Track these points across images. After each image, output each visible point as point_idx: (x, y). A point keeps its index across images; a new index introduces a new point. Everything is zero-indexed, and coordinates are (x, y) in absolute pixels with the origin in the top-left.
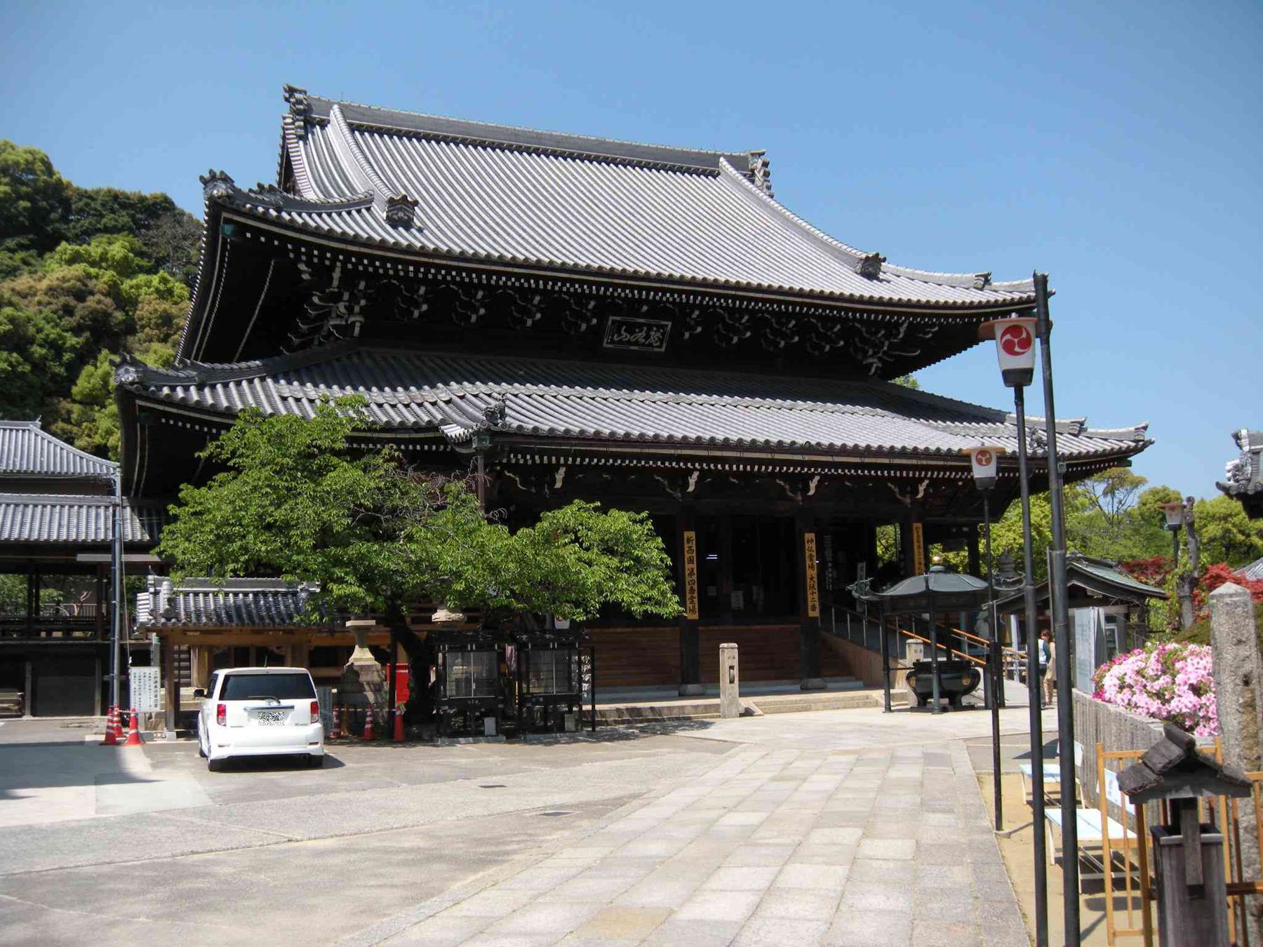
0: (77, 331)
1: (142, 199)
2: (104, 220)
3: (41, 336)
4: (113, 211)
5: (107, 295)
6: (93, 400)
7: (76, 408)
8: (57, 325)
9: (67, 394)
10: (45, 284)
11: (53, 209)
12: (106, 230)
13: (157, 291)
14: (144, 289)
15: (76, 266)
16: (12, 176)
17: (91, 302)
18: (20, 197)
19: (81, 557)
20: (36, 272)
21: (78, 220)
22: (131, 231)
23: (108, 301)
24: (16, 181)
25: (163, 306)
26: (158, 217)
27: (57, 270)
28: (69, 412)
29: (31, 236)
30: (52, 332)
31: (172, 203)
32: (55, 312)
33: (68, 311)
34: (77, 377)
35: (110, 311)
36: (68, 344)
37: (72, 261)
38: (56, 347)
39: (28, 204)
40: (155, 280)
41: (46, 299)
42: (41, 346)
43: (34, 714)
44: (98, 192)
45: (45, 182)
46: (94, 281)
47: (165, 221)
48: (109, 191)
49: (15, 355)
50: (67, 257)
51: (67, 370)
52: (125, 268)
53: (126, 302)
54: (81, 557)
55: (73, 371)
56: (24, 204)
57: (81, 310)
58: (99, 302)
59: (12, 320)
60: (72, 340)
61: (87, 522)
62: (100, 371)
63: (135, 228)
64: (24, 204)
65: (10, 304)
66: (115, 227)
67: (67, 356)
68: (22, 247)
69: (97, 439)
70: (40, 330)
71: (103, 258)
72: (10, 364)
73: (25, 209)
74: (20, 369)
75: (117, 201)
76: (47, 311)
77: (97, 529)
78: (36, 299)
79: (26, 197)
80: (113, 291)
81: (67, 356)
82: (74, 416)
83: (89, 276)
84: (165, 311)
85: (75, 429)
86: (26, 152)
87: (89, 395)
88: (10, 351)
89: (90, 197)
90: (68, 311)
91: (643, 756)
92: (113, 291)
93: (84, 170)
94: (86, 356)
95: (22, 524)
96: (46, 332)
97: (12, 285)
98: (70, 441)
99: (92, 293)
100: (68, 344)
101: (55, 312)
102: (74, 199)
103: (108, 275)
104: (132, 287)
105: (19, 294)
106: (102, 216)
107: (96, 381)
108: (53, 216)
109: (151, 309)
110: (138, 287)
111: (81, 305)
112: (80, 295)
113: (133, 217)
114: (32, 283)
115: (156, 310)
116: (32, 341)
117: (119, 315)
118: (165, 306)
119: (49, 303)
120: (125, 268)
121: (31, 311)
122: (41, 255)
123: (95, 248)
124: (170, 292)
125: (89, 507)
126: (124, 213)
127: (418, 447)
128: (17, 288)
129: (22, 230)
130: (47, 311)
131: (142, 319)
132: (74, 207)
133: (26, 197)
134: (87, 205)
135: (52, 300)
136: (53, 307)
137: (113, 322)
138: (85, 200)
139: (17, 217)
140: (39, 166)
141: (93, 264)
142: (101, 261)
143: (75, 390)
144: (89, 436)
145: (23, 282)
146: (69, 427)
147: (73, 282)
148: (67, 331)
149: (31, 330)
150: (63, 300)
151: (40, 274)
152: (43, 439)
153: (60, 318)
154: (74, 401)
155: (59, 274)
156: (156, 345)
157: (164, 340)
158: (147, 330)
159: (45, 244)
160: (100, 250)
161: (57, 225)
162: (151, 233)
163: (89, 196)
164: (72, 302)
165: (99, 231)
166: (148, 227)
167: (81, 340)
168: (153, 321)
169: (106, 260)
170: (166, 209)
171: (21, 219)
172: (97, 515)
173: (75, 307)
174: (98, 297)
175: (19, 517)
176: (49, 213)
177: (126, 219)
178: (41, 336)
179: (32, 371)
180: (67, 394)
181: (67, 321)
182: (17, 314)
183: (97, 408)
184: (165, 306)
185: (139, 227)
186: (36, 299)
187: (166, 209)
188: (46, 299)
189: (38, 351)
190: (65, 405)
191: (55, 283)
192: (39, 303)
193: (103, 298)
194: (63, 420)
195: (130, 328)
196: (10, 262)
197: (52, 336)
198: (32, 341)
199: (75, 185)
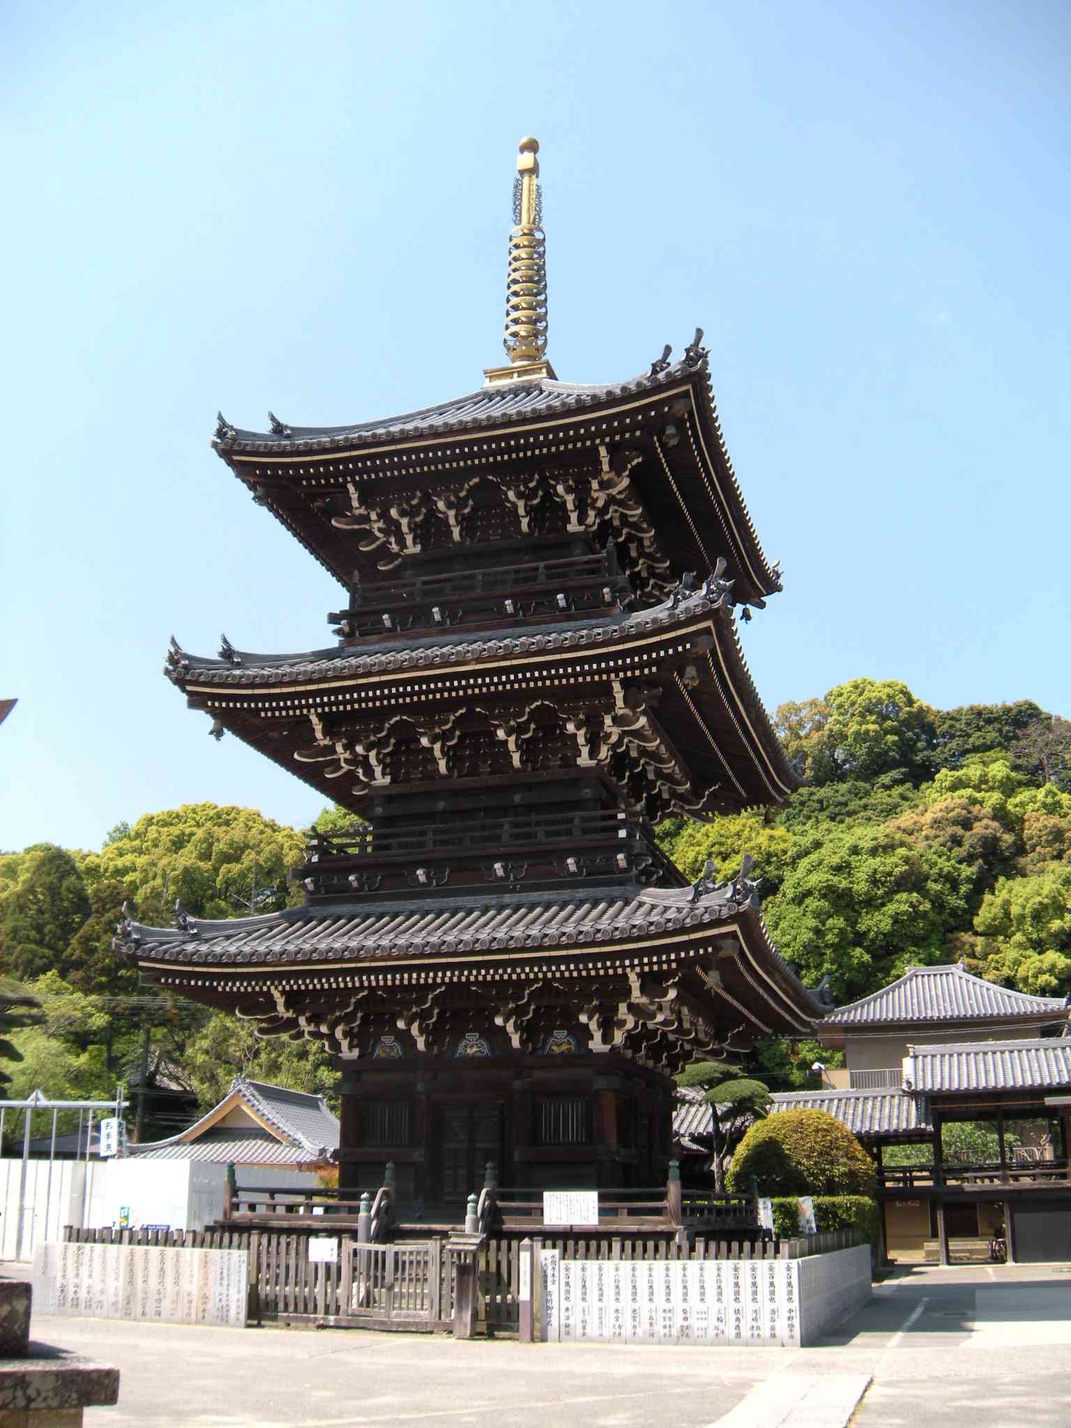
0: (969, 859)
1: (1007, 710)
2: (971, 740)
3: (935, 870)
4: (979, 729)
5: (994, 818)
6: (1000, 929)
7: (980, 941)
8: (949, 859)
9: (969, 927)
10: (929, 817)
11: (919, 739)
12: (975, 749)
13: (1045, 805)
14: (1030, 807)
15: (962, 792)
16: (880, 714)
17: (978, 828)
18: (887, 732)
19: (1050, 1101)
20: (917, 806)
21: (946, 744)
22: (1000, 744)
23: (995, 824)
24: (884, 717)
25: (1052, 821)
26: (1025, 725)
27: (938, 800)
28: (973, 946)
29: (903, 770)
30: (945, 865)
31: (1036, 709)
32: (943, 845)
33: (957, 841)
34: (980, 907)
35: (998, 835)
36: (963, 876)
37: (953, 788)
38: (952, 881)
39: (896, 738)
40: (1041, 794)
41: (933, 832)
42: (935, 881)
43: (1016, 1260)
44: (959, 711)
45: (909, 713)
46: (978, 807)
47: (1033, 730)
48: (971, 709)
49: (915, 894)
50: (947, 784)
51: (967, 902)
52: (1008, 788)
53: (1011, 822)
54: (1050, 1101)
55: (974, 901)
56: (891, 738)
57: (969, 838)
58: (987, 827)
59: (907, 860)
60: (967, 871)
61: (1048, 1065)
62: (999, 901)
63: (1004, 742)
64: (891, 738)
65: (902, 844)
66: (984, 744)
67: (963, 889)
68: (897, 782)
69: (1006, 972)
70: (933, 865)
71: (983, 780)
72: (912, 905)
73: (894, 743)
74: (921, 908)
75: (982, 717)
76: (935, 844)
77: (1059, 1071)
78: (923, 833)
79: (893, 731)
80: (1000, 814)
81: (963, 889)
82: (978, 949)
83: (974, 801)
84: (1055, 826)
85: (981, 964)
86: (884, 686)
87: (989, 927)
88: (910, 891)
89: (953, 718)
90: (957, 841)
91: (171, 1145)
92: (1000, 814)
93: (943, 692)
94: (983, 884)
95: (986, 1072)
96: (939, 866)
97: (897, 822)
98: (979, 975)
99: (977, 819)
100: (963, 876)
101: (943, 845)
102: (937, 723)
103: (995, 797)
104: (1016, 806)
105: (904, 831)
106: (969, 736)
107: (997, 910)
108: (920, 745)
109: (1039, 825)
110: (1022, 804)
111: (968, 834)
112: (967, 824)
113: (1000, 731)
114: (916, 818)
115: (1045, 827)
116: (927, 878)
117: (1009, 838)
118: (1054, 820)
119: (936, 837)
120: (1008, 788)
121: (921, 846)
122: (916, 787)
123: (973, 770)
124: (1058, 804)
125: (1046, 1049)
126: (990, 728)
127: (404, 472)
128: (903, 826)
129: (895, 765)
130: (935, 844)
131: (1031, 838)
132: (938, 731)
133: (893, 731)
134: (951, 726)
135: (938, 833)
136: (941, 839)
137: (1004, 845)
138: (949, 722)
139: (886, 752)
140: (900, 699)
141: (977, 788)
142: (982, 783)
143: (976, 921)
144: (998, 969)
145: (906, 818)
146: (975, 962)
147: (957, 810)
148: (960, 862)
149: (926, 867)
150: (951, 830)
151: (921, 808)
152: (968, 981)
153: (950, 850)
154: (976, 934)
155: (942, 805)
156: (1054, 865)
157: (1059, 856)
158: (1038, 848)
159: (921, 774)
160: (978, 773)
161: (925, 753)
162: (1021, 743)
163: (953, 717)
164: (959, 830)
165: (967, 751)
166: (1017, 738)
167: (974, 869)
168: (1044, 838)
169: (986, 782)
170: (1031, 716)
171: (891, 754)
172: (1056, 1057)
173: (962, 837)
174: (985, 821)
175: (981, 1065)
176: (915, 743)
177: (994, 734)
178: (935, 870)
179: (932, 909)
180: (969, 927)
181: (957, 852)
182: (910, 854)
183: (1001, 938)
184: (1054, 820)
185: (1008, 739)
186: (923, 833)
187: (1031, 716)
188: (933, 832)
189: (934, 887)
190: (967, 937)
191: (939, 815)
192: (927, 838)
193: (990, 823)
194: (968, 956)
195: (1020, 849)
196: (889, 800)
197: (945, 870)
198: (927, 878)
199: (934, 707)
